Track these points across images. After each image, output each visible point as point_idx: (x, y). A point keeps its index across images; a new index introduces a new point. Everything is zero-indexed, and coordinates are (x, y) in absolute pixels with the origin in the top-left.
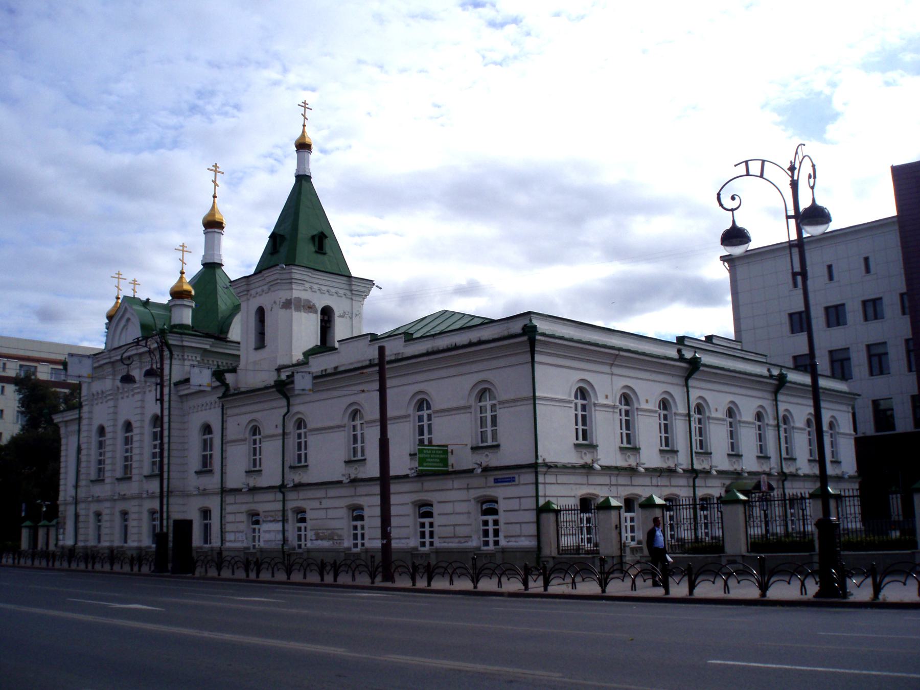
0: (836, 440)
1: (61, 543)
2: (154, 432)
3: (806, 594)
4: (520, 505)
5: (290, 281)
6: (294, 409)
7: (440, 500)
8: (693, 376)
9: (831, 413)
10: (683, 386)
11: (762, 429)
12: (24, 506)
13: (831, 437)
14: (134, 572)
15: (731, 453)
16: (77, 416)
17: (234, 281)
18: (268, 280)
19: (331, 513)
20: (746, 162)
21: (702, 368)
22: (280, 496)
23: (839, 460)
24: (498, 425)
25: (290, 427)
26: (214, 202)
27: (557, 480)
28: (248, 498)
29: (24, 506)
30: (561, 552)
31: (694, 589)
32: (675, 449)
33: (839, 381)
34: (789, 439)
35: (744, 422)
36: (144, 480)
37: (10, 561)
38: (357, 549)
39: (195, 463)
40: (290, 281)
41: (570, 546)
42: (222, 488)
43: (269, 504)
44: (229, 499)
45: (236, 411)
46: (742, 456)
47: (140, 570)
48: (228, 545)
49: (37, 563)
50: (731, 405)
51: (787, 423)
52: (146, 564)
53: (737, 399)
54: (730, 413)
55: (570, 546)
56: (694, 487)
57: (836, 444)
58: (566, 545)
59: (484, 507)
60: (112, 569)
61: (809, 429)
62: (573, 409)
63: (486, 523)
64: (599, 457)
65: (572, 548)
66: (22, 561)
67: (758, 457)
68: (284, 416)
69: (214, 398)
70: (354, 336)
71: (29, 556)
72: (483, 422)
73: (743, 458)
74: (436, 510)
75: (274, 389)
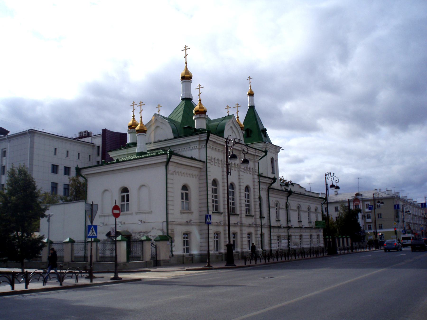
0: (310, 214)
8: (290, 196)
9: (275, 199)
10: (286, 199)
11: (277, 210)
13: (277, 210)
14: (289, 260)
15: (276, 219)
17: (307, 191)
21: (292, 194)
22: (286, 230)
23: (290, 220)
24: (129, 201)
30: (98, 259)
31: (28, 284)
32: (279, 220)
33: (97, 153)
34: (277, 213)
35: (312, 212)
37: (315, 256)
41: (109, 256)
43: (283, 233)
46: (280, 220)
47: (269, 261)
49: (297, 257)
50: (299, 205)
51: (277, 206)
52: (272, 258)
53: (310, 205)
54: (276, 205)
55: (109, 256)
56: (288, 232)
57: (278, 213)
58: (110, 256)
60: (277, 261)
61: (298, 210)
62: (308, 213)
64: (49, 208)
65: (110, 257)
66: (306, 256)
67: (309, 222)
70: (208, 184)
71: (275, 256)
73: (302, 222)
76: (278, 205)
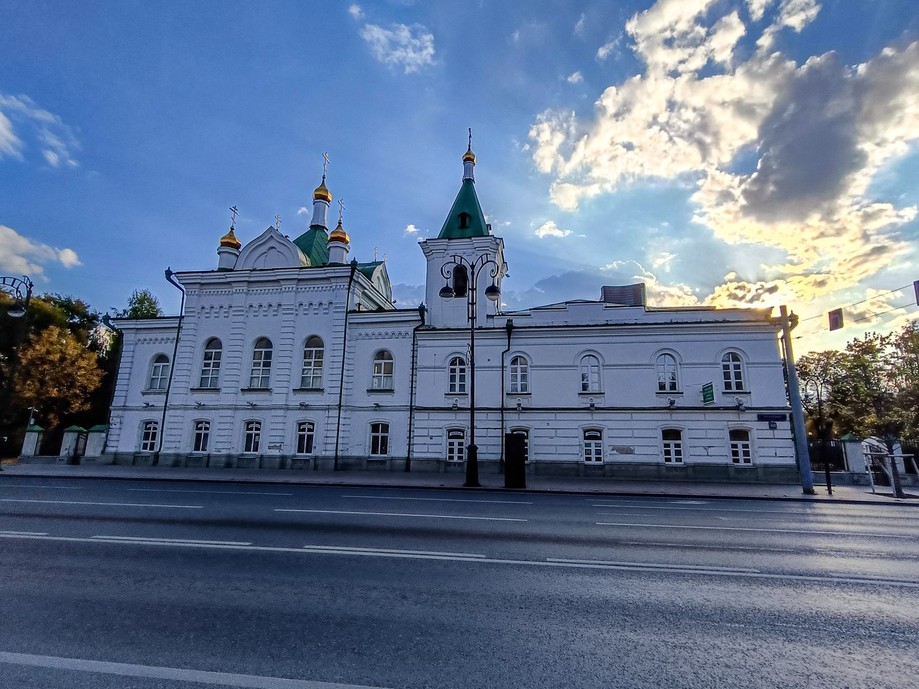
1: (109, 450)
2: (206, 352)
3: (384, 451)
4: (428, 431)
5: (495, 251)
6: (513, 349)
7: (690, 428)
12: (37, 411)
16: (177, 325)
18: (476, 245)
19: (425, 432)
20: (15, 279)
22: (498, 416)
25: (507, 362)
26: (323, 181)
27: (556, 418)
28: (588, 416)
29: (37, 411)
36: (240, 393)
38: (600, 462)
39: (143, 385)
40: (495, 251)
42: (411, 406)
44: (417, 415)
45: (428, 343)
48: (415, 455)
59: (587, 434)
63: (451, 444)
68: (503, 353)
69: (410, 329)
72: (453, 378)
74: (605, 434)
75: (506, 330)
76: (740, 356)
